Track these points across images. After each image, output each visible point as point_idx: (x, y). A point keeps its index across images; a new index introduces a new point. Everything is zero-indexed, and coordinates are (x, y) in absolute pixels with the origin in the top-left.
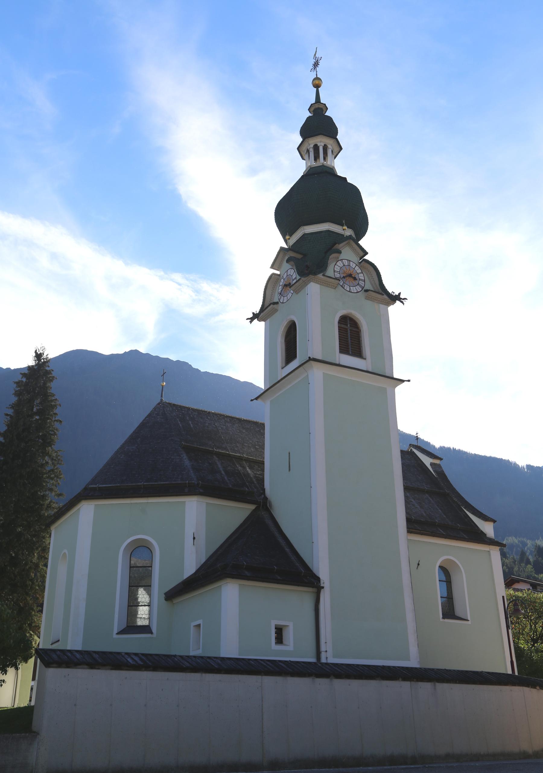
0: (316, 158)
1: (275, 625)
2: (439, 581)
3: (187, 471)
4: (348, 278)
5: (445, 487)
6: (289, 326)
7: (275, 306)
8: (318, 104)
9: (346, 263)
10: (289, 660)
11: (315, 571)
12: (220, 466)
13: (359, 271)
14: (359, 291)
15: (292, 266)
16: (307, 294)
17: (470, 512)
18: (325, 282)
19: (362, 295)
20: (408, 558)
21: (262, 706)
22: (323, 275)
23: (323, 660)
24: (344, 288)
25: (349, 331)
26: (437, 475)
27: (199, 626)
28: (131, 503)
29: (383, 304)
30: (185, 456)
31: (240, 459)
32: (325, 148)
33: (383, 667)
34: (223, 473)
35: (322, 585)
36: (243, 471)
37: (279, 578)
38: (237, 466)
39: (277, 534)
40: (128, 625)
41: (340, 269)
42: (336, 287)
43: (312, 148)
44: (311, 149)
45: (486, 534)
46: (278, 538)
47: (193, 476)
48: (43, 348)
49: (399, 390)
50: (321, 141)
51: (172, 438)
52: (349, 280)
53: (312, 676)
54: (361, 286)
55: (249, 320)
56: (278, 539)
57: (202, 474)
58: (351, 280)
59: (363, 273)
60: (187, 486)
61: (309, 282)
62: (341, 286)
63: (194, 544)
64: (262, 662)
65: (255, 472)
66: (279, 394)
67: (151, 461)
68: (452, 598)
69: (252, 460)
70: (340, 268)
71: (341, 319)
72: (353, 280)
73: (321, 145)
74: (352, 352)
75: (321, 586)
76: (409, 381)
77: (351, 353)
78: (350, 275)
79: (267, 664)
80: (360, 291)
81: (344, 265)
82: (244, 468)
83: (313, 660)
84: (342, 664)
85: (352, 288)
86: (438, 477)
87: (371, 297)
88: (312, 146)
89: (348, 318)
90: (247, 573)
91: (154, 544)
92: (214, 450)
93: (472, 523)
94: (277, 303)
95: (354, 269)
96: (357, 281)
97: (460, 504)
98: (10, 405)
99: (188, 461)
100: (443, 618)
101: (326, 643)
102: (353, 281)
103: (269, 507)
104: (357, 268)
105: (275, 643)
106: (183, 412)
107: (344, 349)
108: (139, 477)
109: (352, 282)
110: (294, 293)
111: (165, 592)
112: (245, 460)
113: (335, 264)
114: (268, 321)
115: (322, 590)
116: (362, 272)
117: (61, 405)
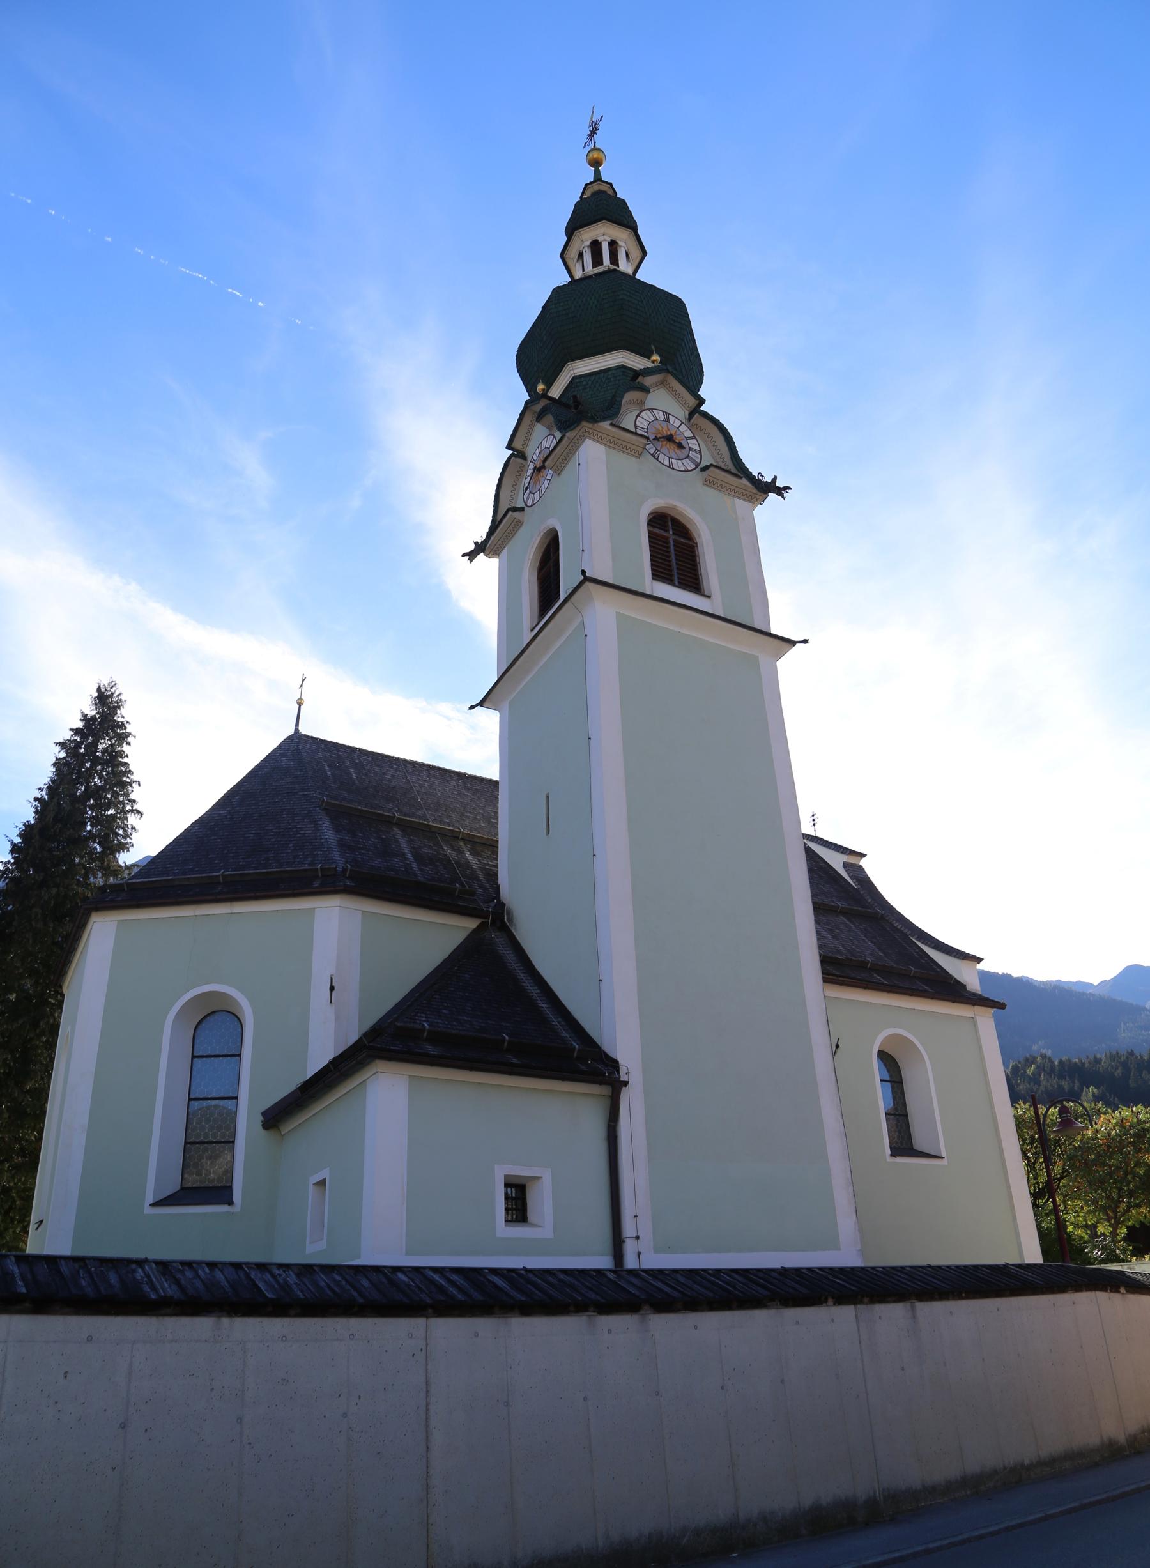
0: (597, 260)
1: (506, 1176)
2: (881, 1080)
3: (325, 849)
5: (876, 905)
6: (542, 550)
7: (517, 515)
9: (661, 417)
10: (520, 1266)
11: (606, 1047)
12: (404, 844)
13: (688, 434)
14: (690, 469)
15: (549, 428)
16: (579, 464)
17: (929, 946)
18: (617, 441)
20: (825, 1016)
21: (427, 1409)
22: (612, 424)
23: (630, 1263)
24: (657, 459)
25: (672, 543)
26: (857, 883)
27: (322, 1183)
28: (196, 916)
29: (740, 498)
30: (326, 823)
31: (454, 836)
32: (613, 244)
33: (784, 1272)
34: (410, 856)
35: (623, 1078)
36: (456, 858)
37: (514, 1060)
38: (446, 848)
39: (522, 975)
40: (184, 1185)
41: (648, 425)
42: (641, 453)
44: (586, 248)
45: (965, 985)
46: (525, 982)
47: (339, 859)
48: (113, 684)
49: (788, 666)
51: (306, 793)
52: (668, 446)
53: (587, 1311)
54: (693, 461)
55: (468, 557)
56: (524, 984)
57: (359, 856)
58: (672, 447)
59: (695, 438)
60: (320, 875)
61: (581, 440)
62: (652, 455)
63: (331, 1002)
64: (436, 1277)
65: (482, 861)
66: (526, 681)
67: (252, 835)
68: (906, 1116)
69: (478, 841)
70: (646, 430)
71: (654, 518)
72: (676, 447)
73: (605, 240)
74: (679, 583)
75: (622, 1079)
76: (805, 641)
77: (677, 583)
78: (670, 438)
79: (449, 1280)
80: (691, 470)
81: (657, 419)
82: (459, 851)
83: (604, 1262)
84: (676, 1271)
85: (674, 461)
86: (859, 887)
87: (715, 481)
88: (588, 243)
89: (669, 518)
90: (430, 1049)
91: (243, 1005)
92: (394, 817)
94: (521, 509)
95: (678, 428)
96: (683, 451)
97: (908, 933)
98: (45, 784)
99: (332, 832)
100: (892, 1155)
101: (636, 1216)
102: (676, 450)
103: (507, 922)
104: (683, 428)
105: (506, 1221)
106: (340, 753)
107: (661, 572)
108: (221, 865)
109: (674, 450)
110: (555, 474)
111: (261, 1112)
112: (462, 839)
113: (638, 415)
114: (504, 553)
115: (624, 1090)
116: (694, 436)
117: (141, 783)
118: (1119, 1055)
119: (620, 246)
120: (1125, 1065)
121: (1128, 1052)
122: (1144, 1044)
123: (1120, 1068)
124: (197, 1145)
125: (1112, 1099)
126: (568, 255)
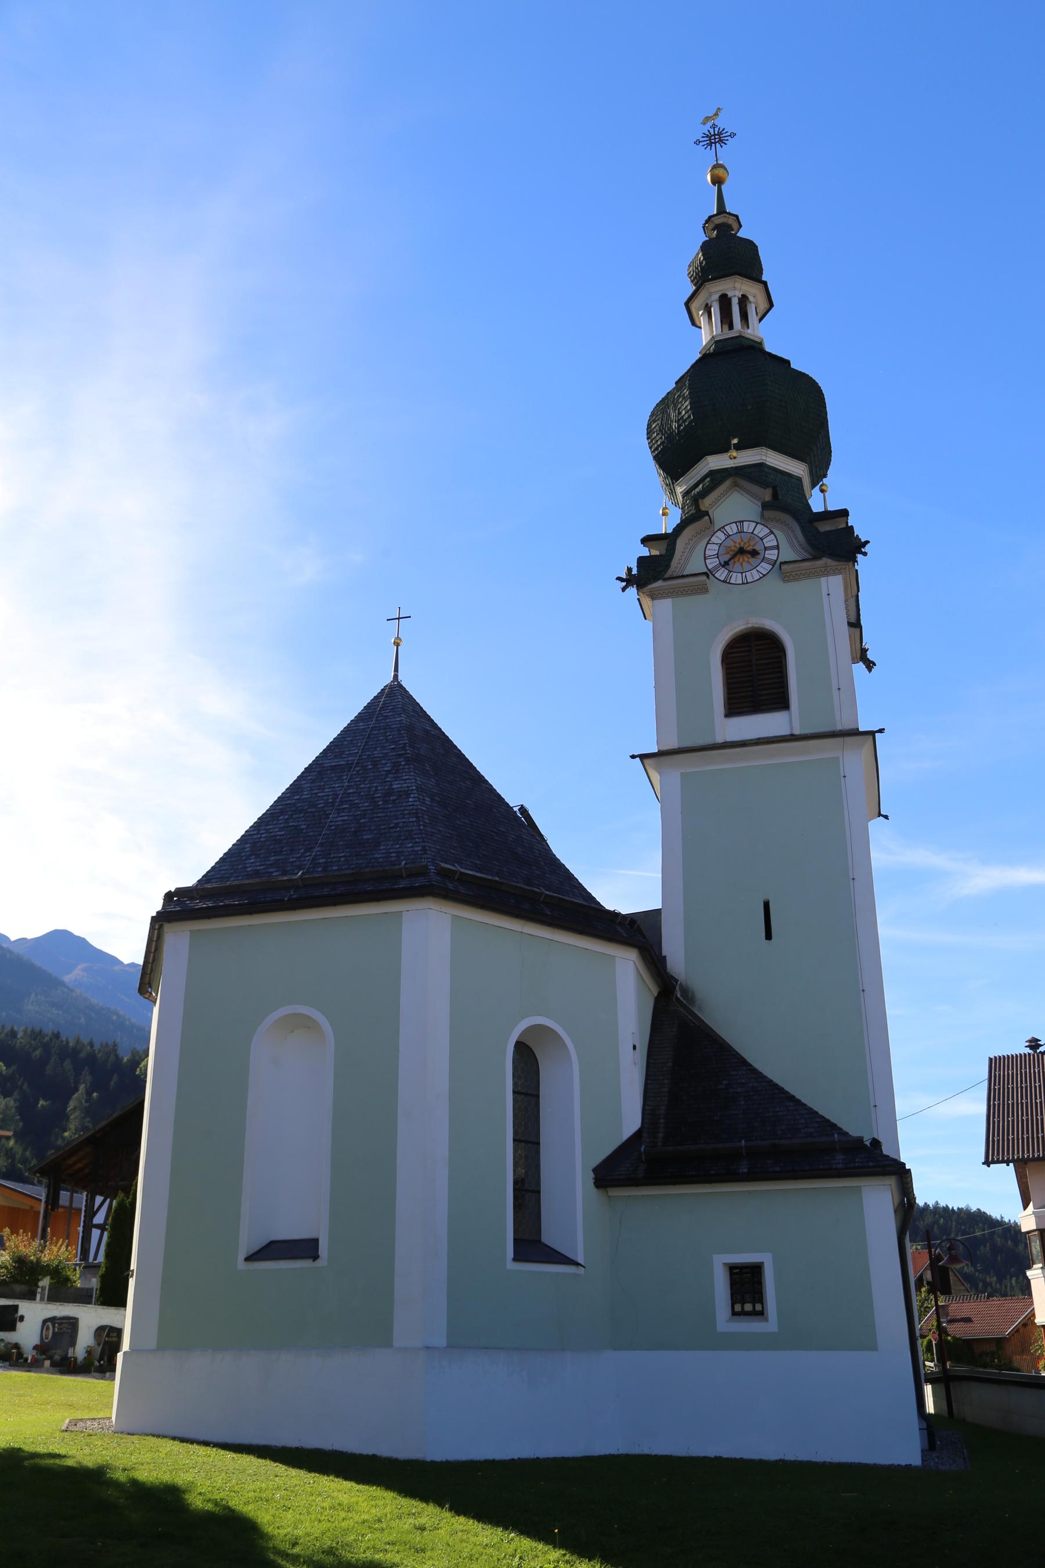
4: (739, 558)
8: (723, 215)
9: (732, 529)
19: (774, 584)
32: (743, 300)
43: (716, 301)
50: (736, 287)
88: (716, 297)
93: (71, 1321)
118: (42, 1034)
119: (750, 302)
120: (46, 1047)
121: (53, 1033)
122: (50, 1024)
123: (40, 1050)
124: (523, 1139)
125: (20, 1083)
126: (694, 306)
